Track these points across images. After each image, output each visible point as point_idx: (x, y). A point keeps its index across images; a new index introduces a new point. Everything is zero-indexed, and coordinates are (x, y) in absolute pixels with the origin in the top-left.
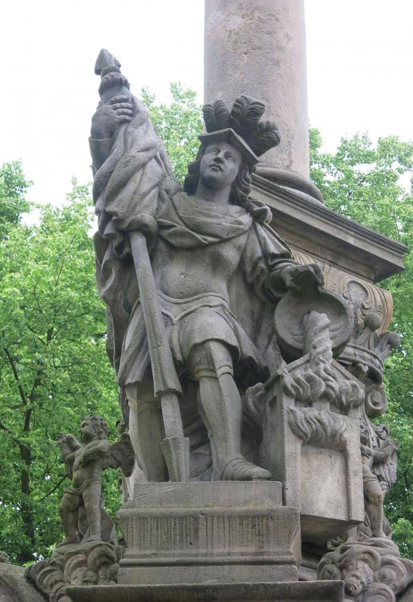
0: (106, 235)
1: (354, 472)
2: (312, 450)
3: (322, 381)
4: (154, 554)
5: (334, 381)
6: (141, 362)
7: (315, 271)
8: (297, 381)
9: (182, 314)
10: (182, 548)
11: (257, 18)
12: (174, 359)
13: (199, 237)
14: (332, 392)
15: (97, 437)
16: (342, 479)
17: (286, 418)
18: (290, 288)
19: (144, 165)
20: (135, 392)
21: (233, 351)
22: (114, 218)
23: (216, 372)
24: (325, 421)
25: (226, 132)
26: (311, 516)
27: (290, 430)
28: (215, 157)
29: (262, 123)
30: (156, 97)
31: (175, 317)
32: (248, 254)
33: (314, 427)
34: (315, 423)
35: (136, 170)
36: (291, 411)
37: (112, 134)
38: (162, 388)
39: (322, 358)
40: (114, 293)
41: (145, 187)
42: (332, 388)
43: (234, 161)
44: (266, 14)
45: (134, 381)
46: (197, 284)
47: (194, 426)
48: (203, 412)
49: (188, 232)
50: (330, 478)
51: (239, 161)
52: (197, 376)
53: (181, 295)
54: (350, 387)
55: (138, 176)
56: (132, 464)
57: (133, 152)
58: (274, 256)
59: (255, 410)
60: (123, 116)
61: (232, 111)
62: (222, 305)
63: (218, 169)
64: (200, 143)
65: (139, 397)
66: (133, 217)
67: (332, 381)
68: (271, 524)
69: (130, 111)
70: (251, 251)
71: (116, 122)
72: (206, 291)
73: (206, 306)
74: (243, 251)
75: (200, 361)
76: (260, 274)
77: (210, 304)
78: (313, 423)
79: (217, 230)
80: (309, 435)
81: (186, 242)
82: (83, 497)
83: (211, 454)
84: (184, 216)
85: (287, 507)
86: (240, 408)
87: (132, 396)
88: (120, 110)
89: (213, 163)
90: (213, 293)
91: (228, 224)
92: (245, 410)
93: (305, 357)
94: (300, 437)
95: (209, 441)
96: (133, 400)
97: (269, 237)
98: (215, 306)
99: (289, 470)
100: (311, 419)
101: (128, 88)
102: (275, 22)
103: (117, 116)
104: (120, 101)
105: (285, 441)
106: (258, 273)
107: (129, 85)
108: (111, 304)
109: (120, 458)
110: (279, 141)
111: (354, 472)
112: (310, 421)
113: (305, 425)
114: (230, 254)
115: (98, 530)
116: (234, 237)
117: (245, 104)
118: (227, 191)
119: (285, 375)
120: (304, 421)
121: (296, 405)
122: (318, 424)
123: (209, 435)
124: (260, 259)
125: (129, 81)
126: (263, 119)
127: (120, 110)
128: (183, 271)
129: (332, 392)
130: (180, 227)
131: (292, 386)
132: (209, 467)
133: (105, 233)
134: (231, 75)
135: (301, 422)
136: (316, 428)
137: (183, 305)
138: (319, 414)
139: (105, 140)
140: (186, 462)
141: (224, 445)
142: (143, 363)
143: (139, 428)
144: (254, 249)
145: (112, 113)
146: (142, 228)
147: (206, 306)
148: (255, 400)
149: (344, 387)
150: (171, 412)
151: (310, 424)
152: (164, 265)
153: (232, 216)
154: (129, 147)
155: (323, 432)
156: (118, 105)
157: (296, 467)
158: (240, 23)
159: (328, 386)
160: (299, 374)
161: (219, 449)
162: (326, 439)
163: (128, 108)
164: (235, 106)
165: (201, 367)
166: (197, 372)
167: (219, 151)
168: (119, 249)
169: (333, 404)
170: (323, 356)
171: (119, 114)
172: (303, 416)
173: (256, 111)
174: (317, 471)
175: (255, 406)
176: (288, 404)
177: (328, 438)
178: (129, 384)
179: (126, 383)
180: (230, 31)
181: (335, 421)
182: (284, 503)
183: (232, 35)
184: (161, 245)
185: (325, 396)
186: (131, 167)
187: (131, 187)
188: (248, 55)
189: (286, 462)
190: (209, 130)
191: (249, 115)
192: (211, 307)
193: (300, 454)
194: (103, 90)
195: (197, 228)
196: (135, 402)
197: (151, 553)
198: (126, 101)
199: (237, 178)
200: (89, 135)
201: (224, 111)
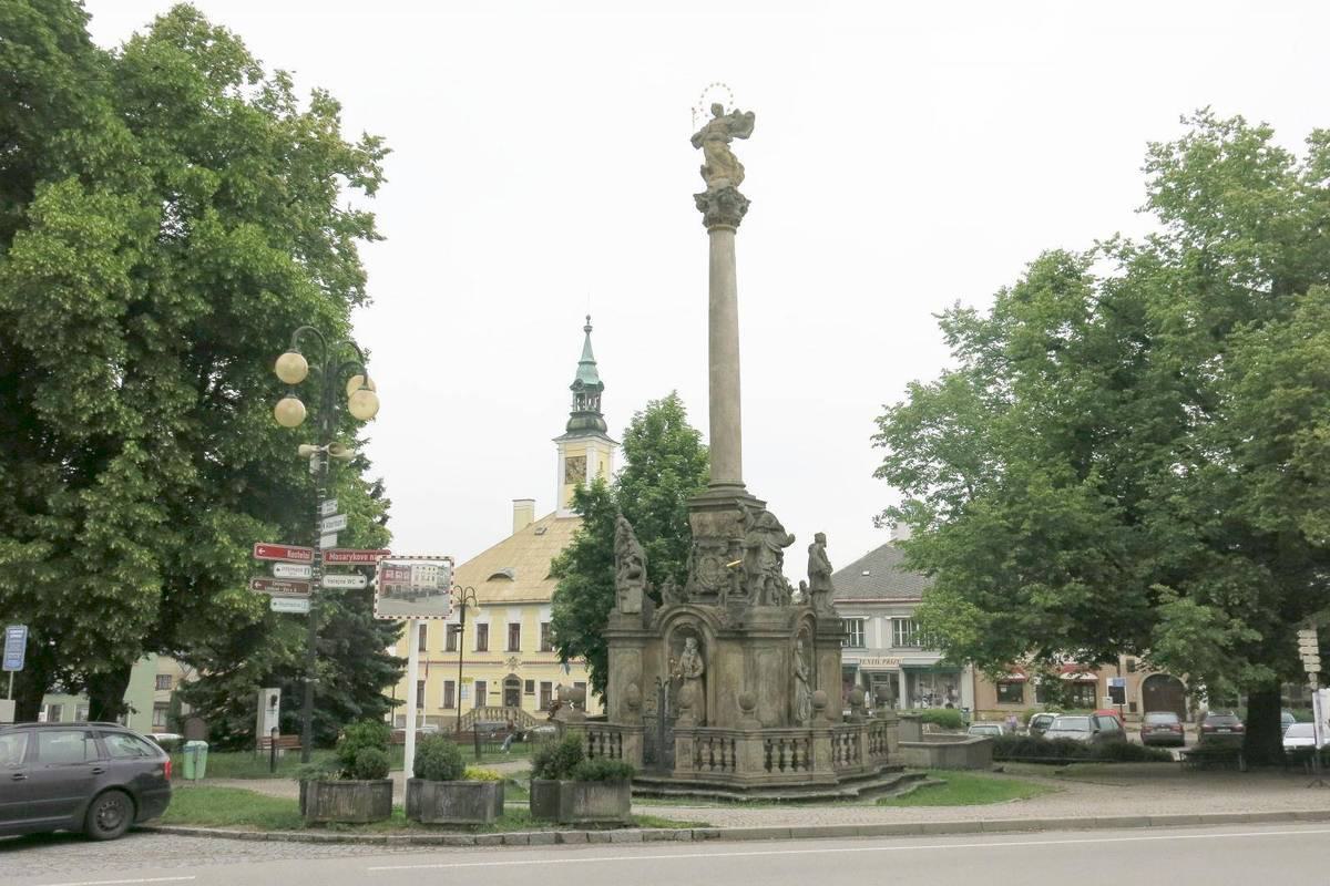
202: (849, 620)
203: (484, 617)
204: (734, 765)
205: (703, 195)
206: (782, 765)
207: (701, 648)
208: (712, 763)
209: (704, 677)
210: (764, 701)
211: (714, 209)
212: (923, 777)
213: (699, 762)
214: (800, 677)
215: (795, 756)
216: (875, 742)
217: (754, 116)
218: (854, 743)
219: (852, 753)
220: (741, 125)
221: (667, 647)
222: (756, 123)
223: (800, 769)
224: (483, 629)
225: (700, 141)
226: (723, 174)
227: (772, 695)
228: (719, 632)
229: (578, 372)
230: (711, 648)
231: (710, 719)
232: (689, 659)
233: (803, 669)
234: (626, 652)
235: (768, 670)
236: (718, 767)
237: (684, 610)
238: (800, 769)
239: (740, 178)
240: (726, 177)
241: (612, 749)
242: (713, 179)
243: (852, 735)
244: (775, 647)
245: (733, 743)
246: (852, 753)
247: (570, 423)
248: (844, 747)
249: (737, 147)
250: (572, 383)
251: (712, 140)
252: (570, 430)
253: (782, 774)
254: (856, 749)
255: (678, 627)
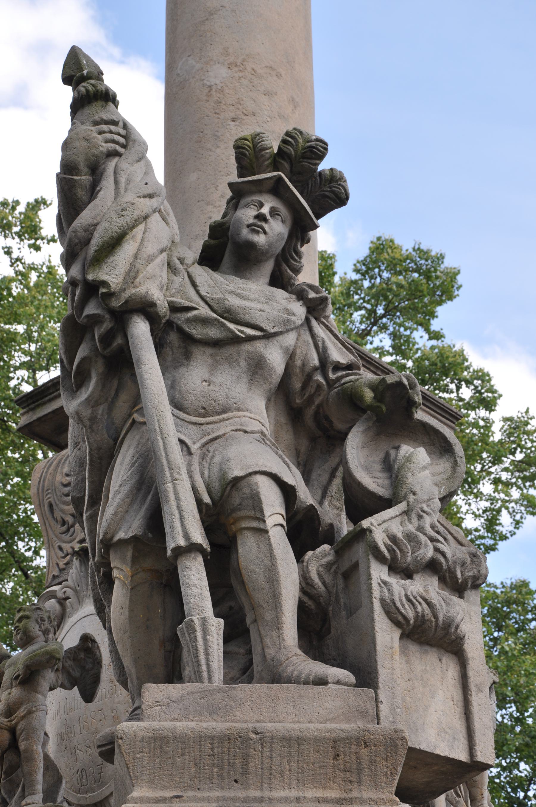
0: (88, 316)
1: (477, 686)
2: (414, 648)
3: (428, 541)
4: (178, 797)
5: (446, 544)
6: (140, 508)
7: (409, 383)
8: (393, 539)
9: (204, 440)
10: (222, 788)
11: (249, 69)
12: (199, 502)
13: (232, 326)
14: (442, 559)
15: (42, 638)
16: (458, 695)
17: (376, 593)
18: (370, 407)
19: (146, 217)
20: (129, 554)
21: (288, 492)
22: (103, 290)
23: (264, 521)
24: (435, 602)
25: (275, 176)
26: (415, 749)
27: (383, 612)
28: (255, 213)
29: (323, 170)
30: (50, 207)
31: (194, 443)
32: (298, 362)
33: (419, 609)
34: (420, 603)
35: (136, 223)
36: (385, 583)
37: (96, 170)
38: (182, 543)
39: (426, 509)
40: (92, 407)
41: (151, 249)
42: (443, 554)
43: (282, 222)
44: (264, 66)
45: (130, 534)
46: (227, 397)
47: (122, 678)
48: (243, 583)
49: (217, 320)
50: (441, 692)
51: (289, 222)
52: (234, 528)
53: (203, 411)
54: (468, 556)
55: (139, 230)
56: (96, 680)
57: (129, 197)
58: (337, 367)
59: (320, 584)
60: (112, 145)
61: (279, 148)
62: (262, 433)
63: (260, 230)
64: (229, 194)
65: (135, 560)
66: (133, 291)
67: (442, 543)
68: (364, 752)
69: (122, 140)
70: (302, 358)
71: (101, 152)
72: (238, 409)
73: (240, 430)
74: (291, 357)
75: (240, 504)
76: (315, 393)
77: (244, 428)
78: (417, 603)
79: (259, 319)
80: (412, 622)
81: (213, 333)
82: (18, 732)
83: (249, 652)
84: (208, 295)
85: (380, 726)
86: (297, 582)
87: (123, 560)
88: (108, 136)
89: (251, 221)
90: (248, 414)
91: (275, 313)
92: (304, 585)
93: (402, 506)
94: (397, 623)
95: (247, 632)
96: (124, 567)
97: (330, 340)
98: (252, 432)
99: (383, 673)
100: (415, 598)
101: (117, 107)
102: (275, 78)
103: (104, 144)
104: (107, 123)
105: (376, 628)
106: (311, 390)
107: (118, 103)
108: (87, 423)
109: (76, 673)
110: (347, 198)
111: (477, 686)
112: (414, 601)
113: (407, 606)
114: (275, 357)
115: (39, 787)
116: (281, 333)
117: (300, 141)
118: (269, 267)
119: (373, 528)
120: (404, 598)
121: (389, 576)
122: (425, 606)
123: (248, 621)
124: (315, 369)
125: (118, 98)
126: (324, 166)
127: (108, 136)
128: (206, 376)
129: (442, 559)
130: (204, 311)
131: (385, 544)
132: (244, 673)
133: (85, 314)
134: (211, 150)
135: (401, 600)
136: (423, 611)
137: (205, 427)
138: (425, 591)
139: (84, 179)
140: (219, 655)
141: (274, 634)
142: (144, 508)
143: (131, 610)
144: (306, 355)
145: (94, 138)
146: (146, 308)
147: (240, 430)
148: (321, 569)
149: (457, 555)
150: (195, 578)
151: (413, 604)
152: (176, 368)
153: (277, 302)
154: (122, 190)
155: (433, 619)
156: (105, 127)
157: (393, 669)
158: (225, 75)
159: (436, 550)
160: (397, 530)
161: (267, 641)
162: (436, 629)
163: (119, 134)
164: (284, 141)
165: (243, 513)
166: (234, 523)
167: (261, 205)
168: (107, 339)
169: (442, 580)
170: (428, 506)
171: (106, 142)
172: (403, 593)
173: (317, 150)
174: (422, 680)
175: (320, 577)
176: (378, 572)
177: (439, 629)
178: (120, 541)
179: (116, 539)
180: (210, 87)
181: (447, 604)
182: (378, 723)
183: (213, 93)
184: (173, 337)
185: (432, 567)
186: (128, 219)
187: (128, 249)
188: (237, 123)
189: (378, 659)
190: (240, 176)
191: (304, 156)
192: (246, 432)
193: (398, 650)
194: (77, 107)
195: (230, 314)
196: (128, 571)
197: (172, 795)
198: (115, 123)
199: (283, 249)
200: (57, 169)
201: (267, 149)
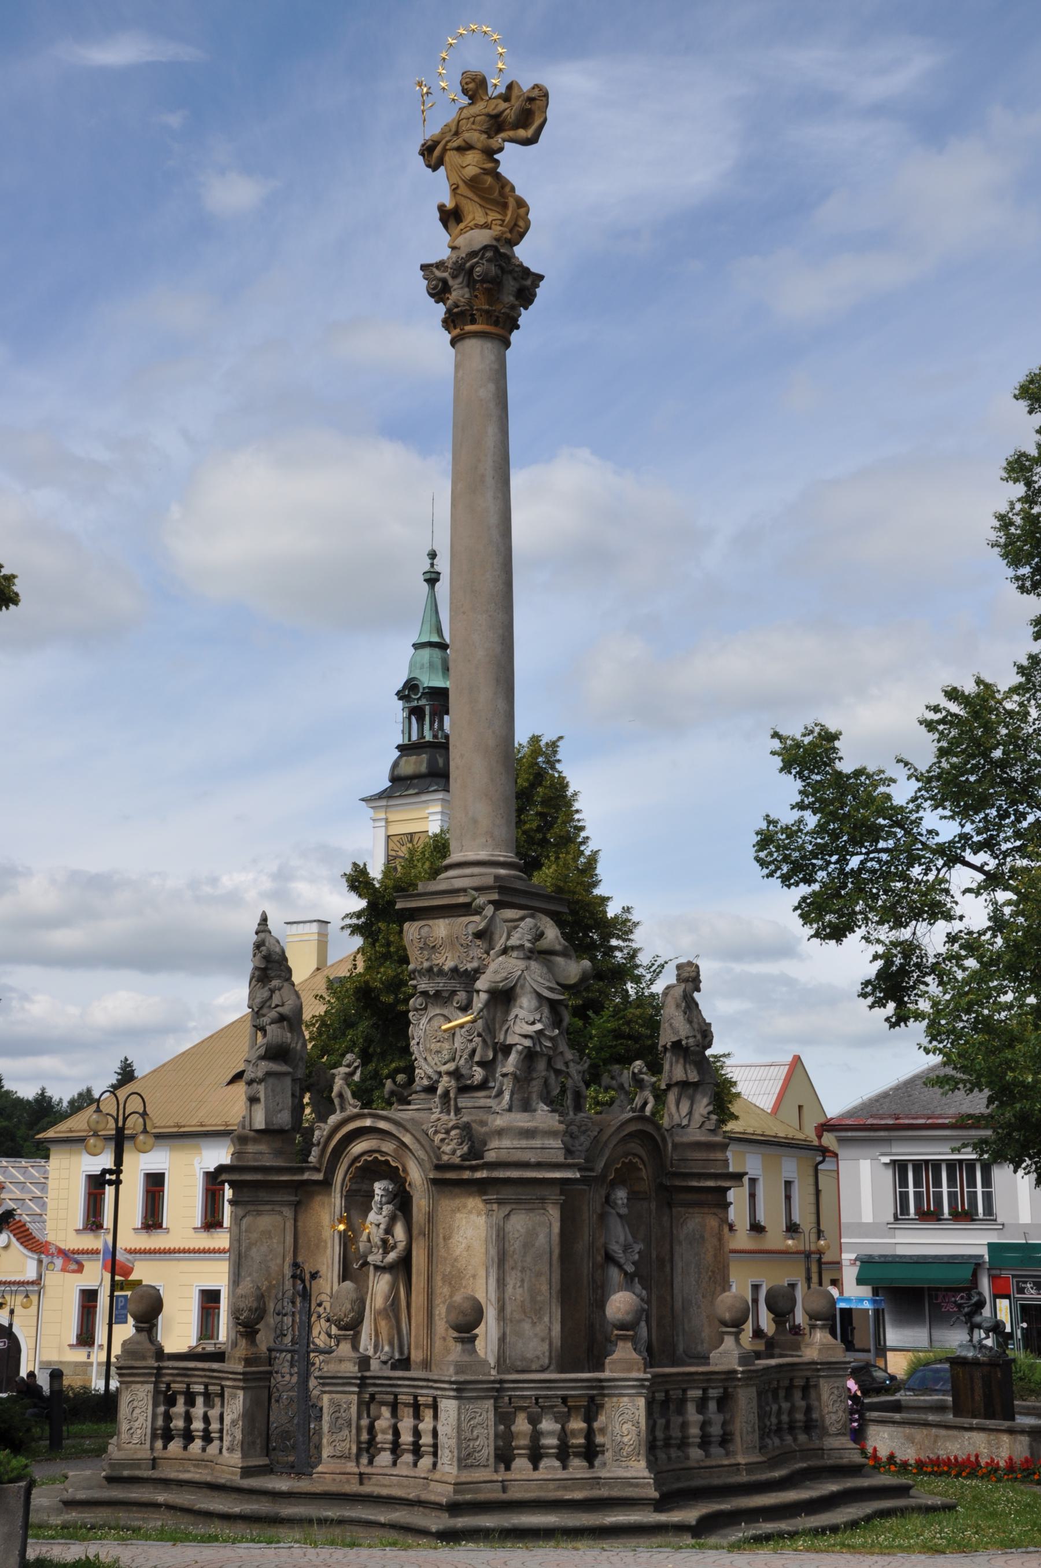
131: (954, 1151)
202: (927, 1161)
203: (156, 1160)
204: (435, 1454)
205: (440, 265)
206: (536, 1457)
207: (402, 1202)
208: (396, 1449)
209: (405, 1264)
210: (517, 1316)
211: (458, 293)
212: (903, 1491)
213: (369, 1448)
214: (620, 1267)
215: (704, 1425)
216: (792, 1411)
217: (546, 95)
218: (720, 1409)
219: (716, 1430)
220: (522, 116)
221: (337, 1199)
222: (550, 113)
223: (576, 1462)
224: (155, 1183)
225: (437, 153)
226: (481, 221)
227: (533, 1300)
228: (438, 1168)
229: (412, 665)
230: (420, 1203)
231: (416, 1356)
232: (378, 1225)
233: (626, 1248)
234: (259, 1213)
235: (527, 1246)
236: (408, 1458)
237: (368, 1122)
238: (576, 1462)
239: (518, 230)
240: (487, 226)
241: (206, 1419)
242: (462, 232)
243: (713, 1393)
244: (543, 1200)
245: (435, 1407)
246: (716, 1430)
247: (396, 765)
248: (692, 1415)
249: (514, 162)
250: (399, 686)
251: (459, 149)
252: (395, 779)
253: (536, 1475)
254: (724, 1424)
255: (357, 1159)
